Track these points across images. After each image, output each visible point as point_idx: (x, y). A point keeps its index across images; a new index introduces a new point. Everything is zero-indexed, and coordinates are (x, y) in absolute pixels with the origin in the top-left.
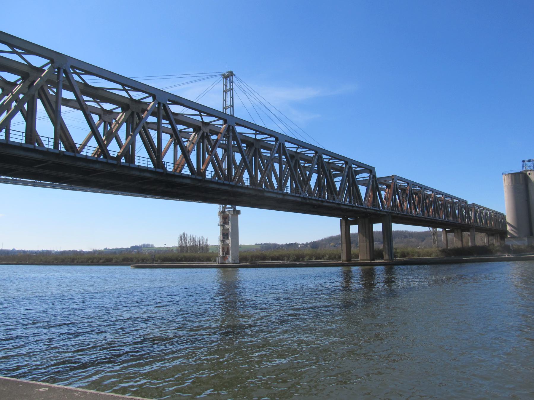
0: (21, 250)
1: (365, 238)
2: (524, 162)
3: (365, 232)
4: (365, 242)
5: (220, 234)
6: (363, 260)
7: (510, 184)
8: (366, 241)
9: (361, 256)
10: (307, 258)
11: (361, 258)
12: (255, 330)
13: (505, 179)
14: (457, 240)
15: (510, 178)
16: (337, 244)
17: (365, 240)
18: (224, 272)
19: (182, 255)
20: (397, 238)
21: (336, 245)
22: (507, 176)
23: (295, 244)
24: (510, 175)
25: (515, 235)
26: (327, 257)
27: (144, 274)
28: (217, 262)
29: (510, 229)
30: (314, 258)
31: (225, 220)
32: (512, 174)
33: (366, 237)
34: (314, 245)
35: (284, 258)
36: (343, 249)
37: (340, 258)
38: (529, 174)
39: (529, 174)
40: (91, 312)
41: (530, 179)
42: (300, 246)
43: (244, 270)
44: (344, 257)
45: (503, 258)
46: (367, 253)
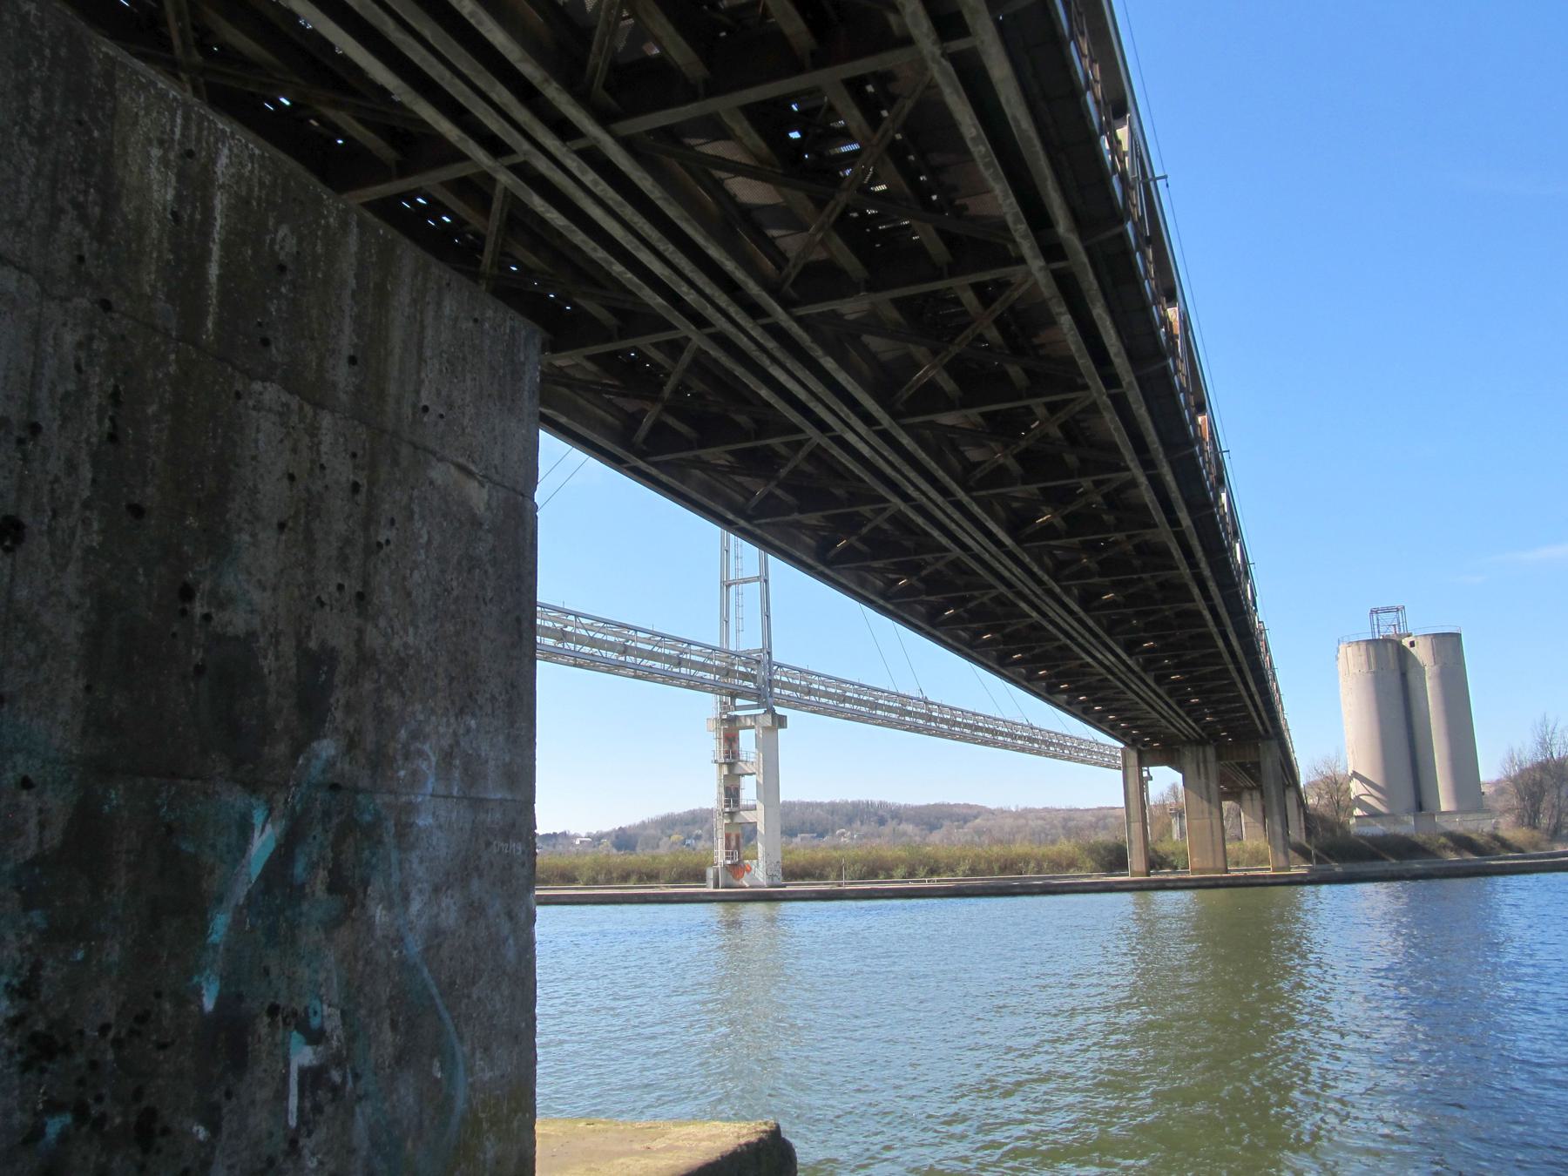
0: (899, 807)
1: (1205, 804)
2: (1374, 612)
3: (1208, 787)
4: (1207, 815)
5: (715, 795)
6: (1202, 871)
7: (1365, 669)
8: (1211, 813)
9: (1195, 859)
10: (901, 871)
11: (1197, 866)
12: (1407, 1089)
13: (1350, 655)
14: (1251, 820)
15: (1363, 652)
16: (689, 837)
17: (1206, 811)
18: (727, 911)
19: (618, 858)
20: (859, 823)
21: (688, 842)
22: (1356, 648)
23: (564, 834)
24: (1363, 646)
25: (1382, 808)
26: (965, 867)
27: (622, 912)
28: (711, 883)
29: (1367, 792)
30: (922, 871)
31: (731, 746)
32: (1435, 636)
33: (1209, 801)
34: (624, 839)
35: (825, 873)
36: (1133, 839)
37: (700, 877)
38: (1412, 644)
39: (1412, 644)
40: (1050, 1027)
41: (1415, 659)
42: (578, 842)
43: (892, 908)
44: (1136, 861)
45: (1493, 865)
46: (1214, 851)
